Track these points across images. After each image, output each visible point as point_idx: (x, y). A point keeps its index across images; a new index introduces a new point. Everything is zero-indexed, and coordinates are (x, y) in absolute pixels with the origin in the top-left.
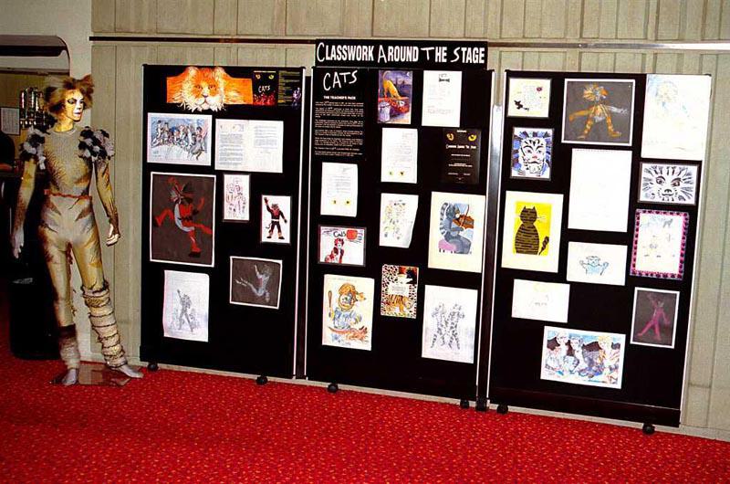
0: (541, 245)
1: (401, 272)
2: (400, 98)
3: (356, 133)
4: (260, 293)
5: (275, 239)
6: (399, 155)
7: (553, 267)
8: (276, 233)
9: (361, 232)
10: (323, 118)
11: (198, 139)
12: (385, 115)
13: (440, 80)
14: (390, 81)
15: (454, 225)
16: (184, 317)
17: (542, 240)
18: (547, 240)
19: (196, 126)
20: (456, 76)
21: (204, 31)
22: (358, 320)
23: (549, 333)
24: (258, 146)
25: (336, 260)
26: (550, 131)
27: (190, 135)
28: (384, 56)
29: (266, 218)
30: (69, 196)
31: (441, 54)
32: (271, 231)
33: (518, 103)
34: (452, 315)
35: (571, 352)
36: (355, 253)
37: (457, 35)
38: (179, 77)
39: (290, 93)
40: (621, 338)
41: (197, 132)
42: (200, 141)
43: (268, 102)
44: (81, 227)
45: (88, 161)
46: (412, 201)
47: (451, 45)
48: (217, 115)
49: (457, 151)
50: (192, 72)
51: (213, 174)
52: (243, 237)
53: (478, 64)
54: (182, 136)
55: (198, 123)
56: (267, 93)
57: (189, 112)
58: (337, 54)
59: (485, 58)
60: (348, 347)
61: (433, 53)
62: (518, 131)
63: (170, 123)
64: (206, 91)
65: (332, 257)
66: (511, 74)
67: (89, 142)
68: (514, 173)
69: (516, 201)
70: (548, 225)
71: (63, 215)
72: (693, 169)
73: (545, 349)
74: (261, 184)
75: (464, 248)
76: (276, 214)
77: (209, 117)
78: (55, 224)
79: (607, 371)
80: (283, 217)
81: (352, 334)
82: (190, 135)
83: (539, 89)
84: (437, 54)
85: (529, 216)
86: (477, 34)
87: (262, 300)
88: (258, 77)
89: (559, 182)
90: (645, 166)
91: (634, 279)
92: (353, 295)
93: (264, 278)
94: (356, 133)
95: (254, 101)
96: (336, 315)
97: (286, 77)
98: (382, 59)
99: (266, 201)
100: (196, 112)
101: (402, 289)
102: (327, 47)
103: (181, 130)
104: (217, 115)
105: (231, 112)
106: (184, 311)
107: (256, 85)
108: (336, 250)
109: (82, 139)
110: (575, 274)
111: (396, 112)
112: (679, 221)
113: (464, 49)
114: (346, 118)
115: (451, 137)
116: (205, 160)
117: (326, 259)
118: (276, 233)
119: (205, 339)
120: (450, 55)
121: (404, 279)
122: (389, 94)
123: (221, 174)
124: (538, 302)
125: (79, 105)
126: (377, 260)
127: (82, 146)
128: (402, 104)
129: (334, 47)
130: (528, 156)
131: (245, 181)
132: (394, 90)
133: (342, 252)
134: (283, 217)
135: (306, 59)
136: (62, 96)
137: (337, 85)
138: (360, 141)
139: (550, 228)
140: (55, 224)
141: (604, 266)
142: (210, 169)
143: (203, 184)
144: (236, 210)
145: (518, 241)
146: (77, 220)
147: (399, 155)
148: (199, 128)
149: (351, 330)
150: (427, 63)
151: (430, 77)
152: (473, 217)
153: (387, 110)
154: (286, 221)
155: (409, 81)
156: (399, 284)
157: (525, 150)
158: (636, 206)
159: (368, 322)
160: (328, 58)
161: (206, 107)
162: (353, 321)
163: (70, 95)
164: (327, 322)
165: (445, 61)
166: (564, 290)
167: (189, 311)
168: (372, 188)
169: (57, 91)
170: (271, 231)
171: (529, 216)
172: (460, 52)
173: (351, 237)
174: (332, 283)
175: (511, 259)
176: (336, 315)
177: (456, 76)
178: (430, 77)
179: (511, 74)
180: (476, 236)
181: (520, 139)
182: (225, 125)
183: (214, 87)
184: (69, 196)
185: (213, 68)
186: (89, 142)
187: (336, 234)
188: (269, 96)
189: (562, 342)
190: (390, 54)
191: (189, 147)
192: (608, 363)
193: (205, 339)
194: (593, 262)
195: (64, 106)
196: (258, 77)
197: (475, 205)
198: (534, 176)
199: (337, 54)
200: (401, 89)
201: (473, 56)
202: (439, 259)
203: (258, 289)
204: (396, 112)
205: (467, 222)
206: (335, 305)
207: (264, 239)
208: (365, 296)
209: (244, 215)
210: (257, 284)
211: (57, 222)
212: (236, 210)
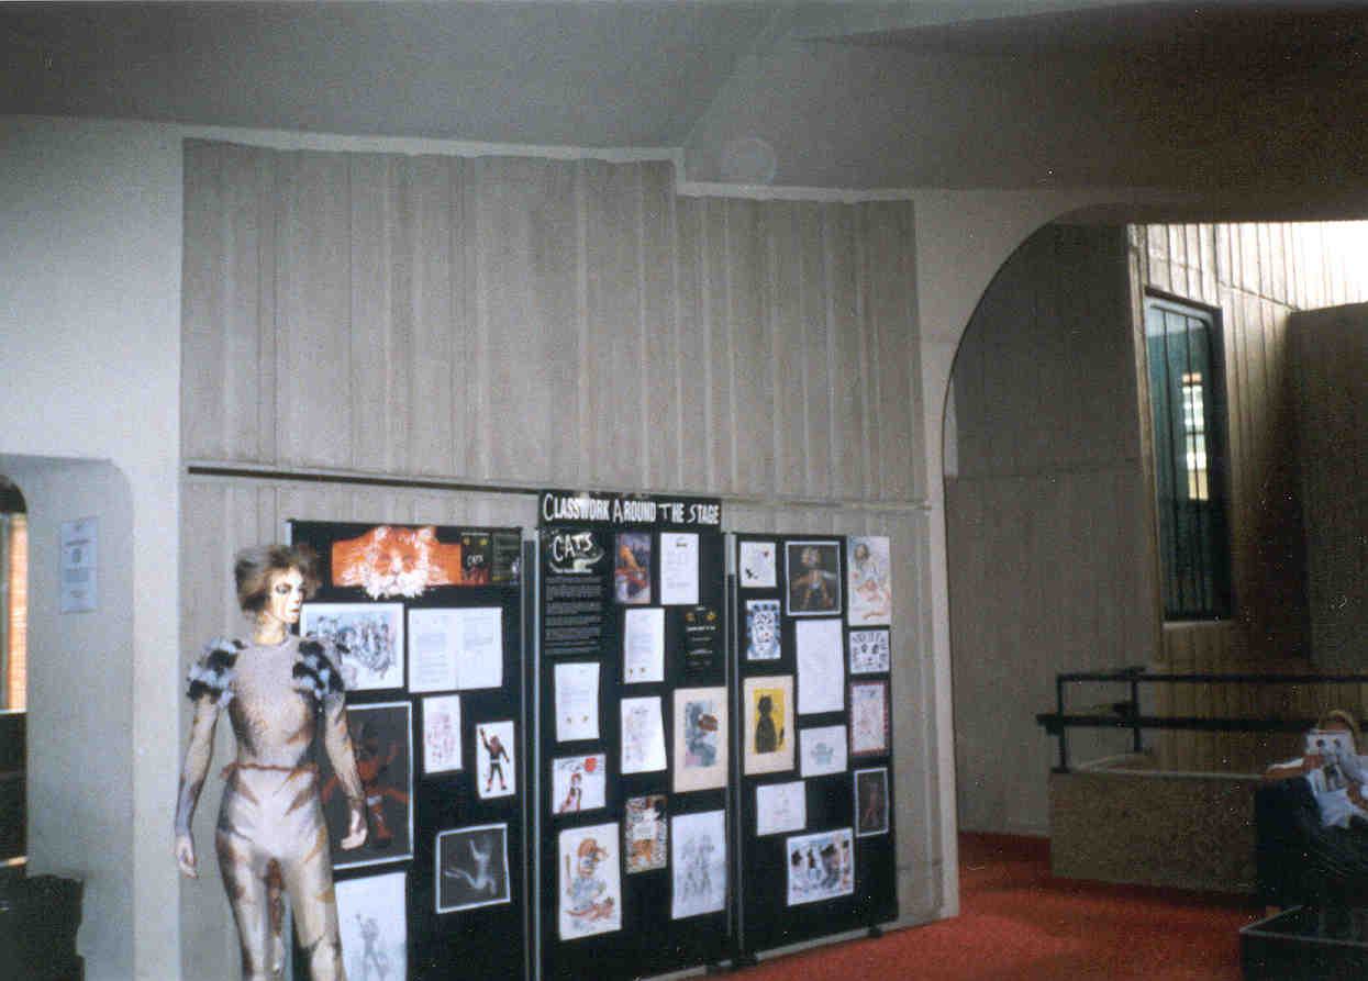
0: (778, 740)
1: (647, 806)
2: (638, 569)
3: (592, 619)
4: (480, 883)
5: (496, 792)
6: (646, 644)
7: (788, 765)
8: (495, 783)
9: (600, 759)
10: (560, 600)
11: (382, 645)
12: (623, 596)
13: (678, 545)
14: (629, 547)
15: (698, 730)
16: (370, 961)
17: (778, 732)
18: (782, 733)
19: (380, 623)
20: (692, 540)
21: (387, 466)
22: (601, 888)
23: (792, 844)
24: (465, 648)
25: (572, 808)
26: (777, 603)
27: (371, 639)
28: (620, 514)
29: (483, 760)
30: (274, 768)
31: (677, 514)
32: (490, 781)
33: (748, 571)
34: (701, 850)
35: (812, 864)
36: (593, 794)
37: (696, 489)
38: (354, 543)
39: (507, 566)
40: (847, 833)
41: (382, 633)
42: (385, 648)
43: (481, 581)
44: (294, 828)
45: (308, 695)
46: (654, 704)
47: (688, 501)
48: (410, 603)
49: (696, 634)
50: (380, 534)
51: (407, 700)
52: (451, 798)
53: (714, 525)
54: (359, 641)
55: (382, 617)
56: (479, 565)
57: (369, 600)
58: (568, 510)
59: (719, 518)
60: (591, 933)
61: (669, 510)
62: (750, 604)
63: (340, 621)
64: (397, 563)
65: (568, 802)
66: (741, 537)
67: (312, 661)
68: (750, 657)
69: (754, 687)
70: (782, 717)
71: (265, 804)
72: (885, 634)
73: (791, 868)
74: (478, 707)
75: (708, 757)
76: (496, 750)
77: (399, 608)
78: (248, 824)
79: (842, 875)
80: (505, 756)
81: (594, 913)
82: (371, 639)
83: (766, 554)
84: (674, 513)
85: (765, 705)
86: (711, 490)
87: (486, 895)
88: (467, 541)
89: (786, 664)
90: (853, 635)
91: (855, 761)
92: (592, 852)
93: (481, 858)
94: (592, 619)
95: (463, 578)
96: (575, 890)
97: (503, 542)
98: (618, 518)
99: (483, 734)
100: (382, 599)
101: (648, 830)
102: (556, 500)
103: (359, 632)
104: (410, 603)
105: (434, 598)
106: (369, 950)
107: (467, 552)
108: (572, 792)
109: (301, 658)
110: (810, 768)
111: (634, 589)
112: (879, 688)
113: (700, 507)
114: (583, 599)
115: (690, 617)
116: (393, 680)
117: (563, 808)
118: (495, 783)
119: (794, 899)
120: (686, 515)
121: (651, 814)
122: (626, 563)
123: (417, 700)
124: (780, 809)
125: (295, 595)
126: (624, 790)
127: (300, 670)
128: (640, 576)
129: (564, 500)
130: (761, 633)
131: (453, 706)
132: (631, 558)
133: (580, 792)
134: (505, 756)
135: (521, 515)
136: (267, 580)
137: (569, 553)
138: (597, 631)
139: (784, 721)
140: (248, 824)
141: (825, 754)
142: (400, 693)
143: (386, 725)
144: (442, 755)
145: (759, 738)
146: (288, 813)
147: (646, 644)
148: (385, 627)
149: (595, 907)
150: (663, 524)
151: (667, 540)
152: (717, 718)
153: (624, 586)
154: (508, 761)
155: (647, 547)
156: (645, 824)
157: (758, 626)
158: (851, 680)
159: (613, 890)
160: (557, 516)
161: (394, 591)
162: (595, 892)
163: (279, 579)
164: (566, 903)
165: (681, 520)
166: (800, 787)
167: (376, 947)
168: (613, 691)
169: (259, 570)
170: (490, 781)
171: (765, 705)
172: (696, 510)
173: (589, 767)
174: (570, 840)
175: (755, 763)
176: (573, 894)
177: (692, 540)
178: (667, 540)
179: (741, 537)
180: (719, 739)
181: (752, 615)
182: (426, 620)
183: (410, 558)
184: (274, 768)
185: (414, 528)
186: (312, 661)
187: (574, 768)
188: (483, 572)
189: (803, 854)
190: (626, 511)
191: (369, 659)
192: (843, 866)
193: (794, 899)
194: (822, 752)
195: (269, 598)
196: (467, 541)
197: (713, 699)
198: (767, 657)
199: (568, 510)
200: (638, 554)
201: (707, 515)
202: (684, 782)
203: (476, 880)
204: (634, 589)
205: (709, 723)
206: (574, 875)
207: (483, 794)
208: (607, 851)
209: (454, 762)
210: (472, 867)
211: (251, 817)
212: (442, 755)
